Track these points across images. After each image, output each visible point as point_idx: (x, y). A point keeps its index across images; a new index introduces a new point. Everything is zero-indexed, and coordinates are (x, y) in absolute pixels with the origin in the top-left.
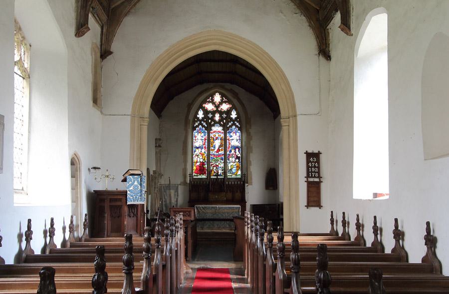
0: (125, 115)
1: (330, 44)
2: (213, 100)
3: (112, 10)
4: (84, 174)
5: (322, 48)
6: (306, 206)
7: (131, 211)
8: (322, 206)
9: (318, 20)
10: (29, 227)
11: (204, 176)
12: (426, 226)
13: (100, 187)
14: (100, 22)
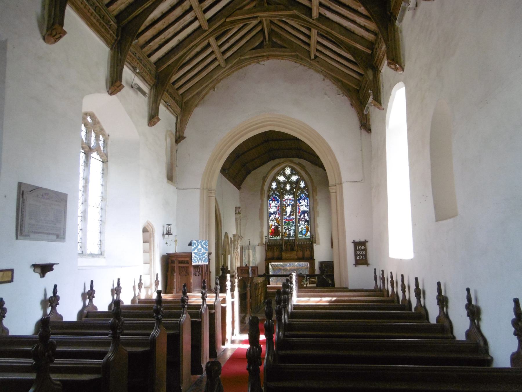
0: (195, 189)
1: (371, 119)
2: (284, 172)
3: (185, 102)
4: (158, 238)
5: (363, 123)
6: (354, 265)
7: (196, 270)
8: (369, 264)
9: (358, 99)
10: (92, 287)
11: (278, 238)
12: (436, 286)
13: (172, 250)
14: (174, 113)
